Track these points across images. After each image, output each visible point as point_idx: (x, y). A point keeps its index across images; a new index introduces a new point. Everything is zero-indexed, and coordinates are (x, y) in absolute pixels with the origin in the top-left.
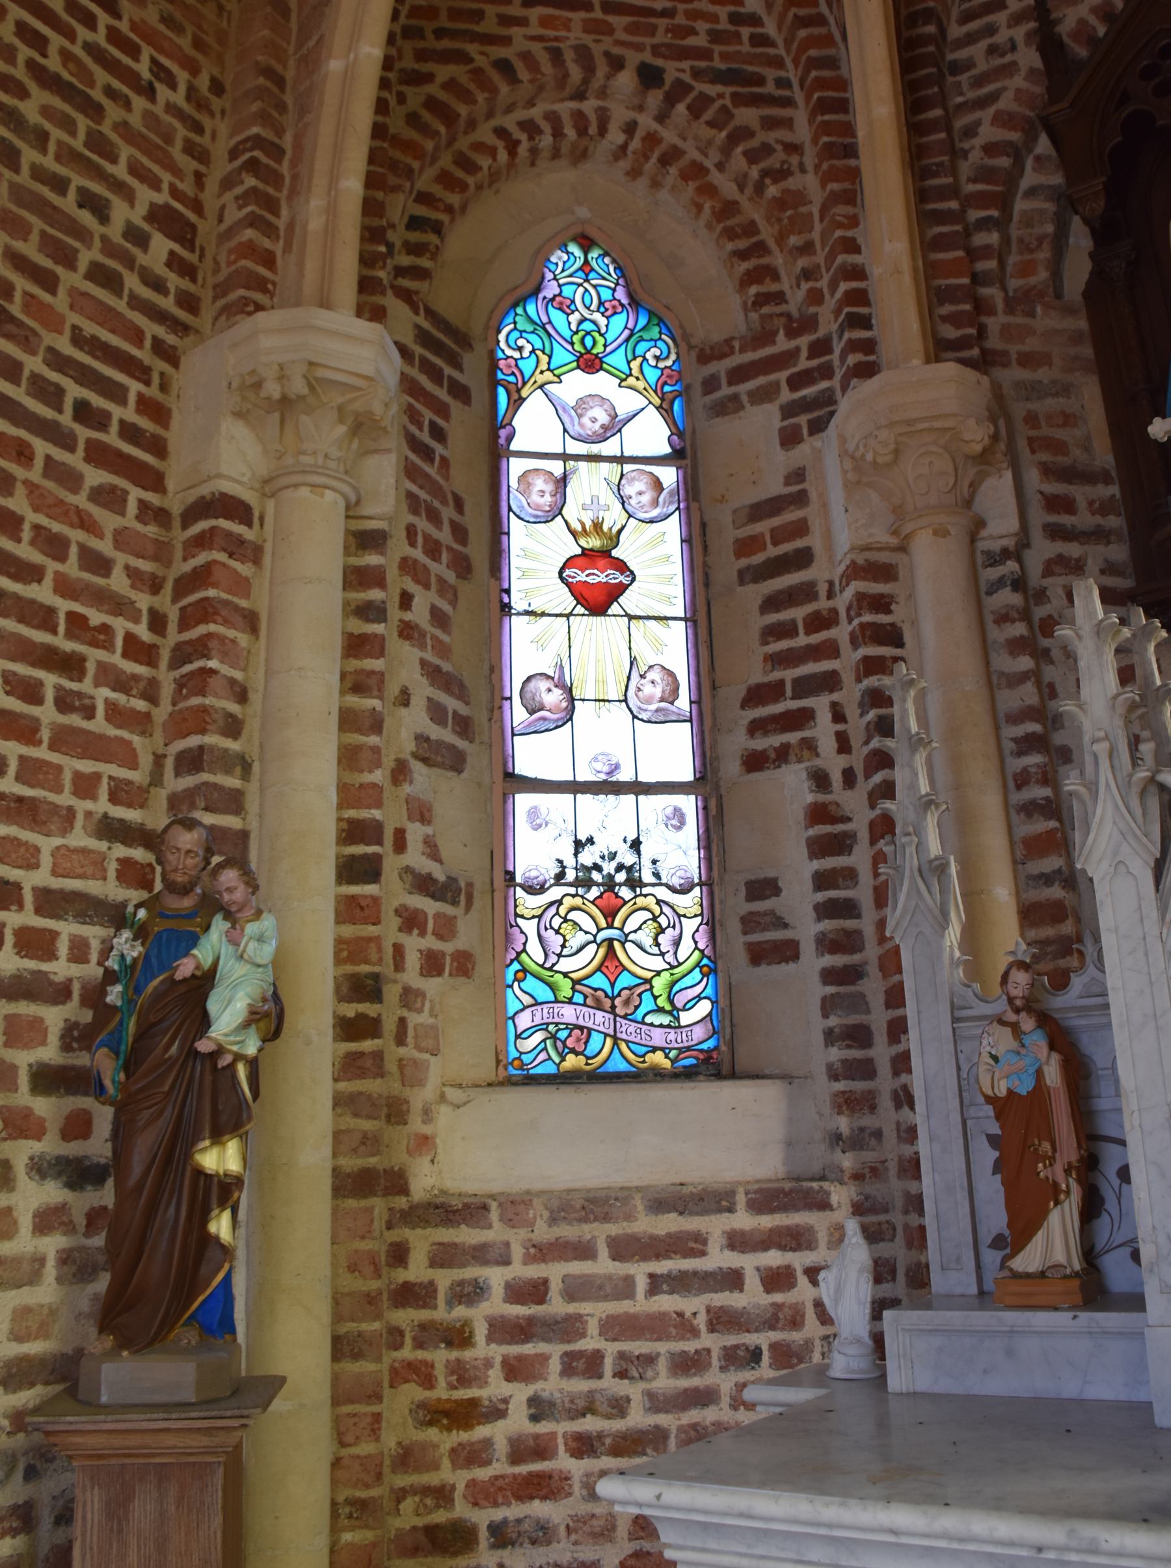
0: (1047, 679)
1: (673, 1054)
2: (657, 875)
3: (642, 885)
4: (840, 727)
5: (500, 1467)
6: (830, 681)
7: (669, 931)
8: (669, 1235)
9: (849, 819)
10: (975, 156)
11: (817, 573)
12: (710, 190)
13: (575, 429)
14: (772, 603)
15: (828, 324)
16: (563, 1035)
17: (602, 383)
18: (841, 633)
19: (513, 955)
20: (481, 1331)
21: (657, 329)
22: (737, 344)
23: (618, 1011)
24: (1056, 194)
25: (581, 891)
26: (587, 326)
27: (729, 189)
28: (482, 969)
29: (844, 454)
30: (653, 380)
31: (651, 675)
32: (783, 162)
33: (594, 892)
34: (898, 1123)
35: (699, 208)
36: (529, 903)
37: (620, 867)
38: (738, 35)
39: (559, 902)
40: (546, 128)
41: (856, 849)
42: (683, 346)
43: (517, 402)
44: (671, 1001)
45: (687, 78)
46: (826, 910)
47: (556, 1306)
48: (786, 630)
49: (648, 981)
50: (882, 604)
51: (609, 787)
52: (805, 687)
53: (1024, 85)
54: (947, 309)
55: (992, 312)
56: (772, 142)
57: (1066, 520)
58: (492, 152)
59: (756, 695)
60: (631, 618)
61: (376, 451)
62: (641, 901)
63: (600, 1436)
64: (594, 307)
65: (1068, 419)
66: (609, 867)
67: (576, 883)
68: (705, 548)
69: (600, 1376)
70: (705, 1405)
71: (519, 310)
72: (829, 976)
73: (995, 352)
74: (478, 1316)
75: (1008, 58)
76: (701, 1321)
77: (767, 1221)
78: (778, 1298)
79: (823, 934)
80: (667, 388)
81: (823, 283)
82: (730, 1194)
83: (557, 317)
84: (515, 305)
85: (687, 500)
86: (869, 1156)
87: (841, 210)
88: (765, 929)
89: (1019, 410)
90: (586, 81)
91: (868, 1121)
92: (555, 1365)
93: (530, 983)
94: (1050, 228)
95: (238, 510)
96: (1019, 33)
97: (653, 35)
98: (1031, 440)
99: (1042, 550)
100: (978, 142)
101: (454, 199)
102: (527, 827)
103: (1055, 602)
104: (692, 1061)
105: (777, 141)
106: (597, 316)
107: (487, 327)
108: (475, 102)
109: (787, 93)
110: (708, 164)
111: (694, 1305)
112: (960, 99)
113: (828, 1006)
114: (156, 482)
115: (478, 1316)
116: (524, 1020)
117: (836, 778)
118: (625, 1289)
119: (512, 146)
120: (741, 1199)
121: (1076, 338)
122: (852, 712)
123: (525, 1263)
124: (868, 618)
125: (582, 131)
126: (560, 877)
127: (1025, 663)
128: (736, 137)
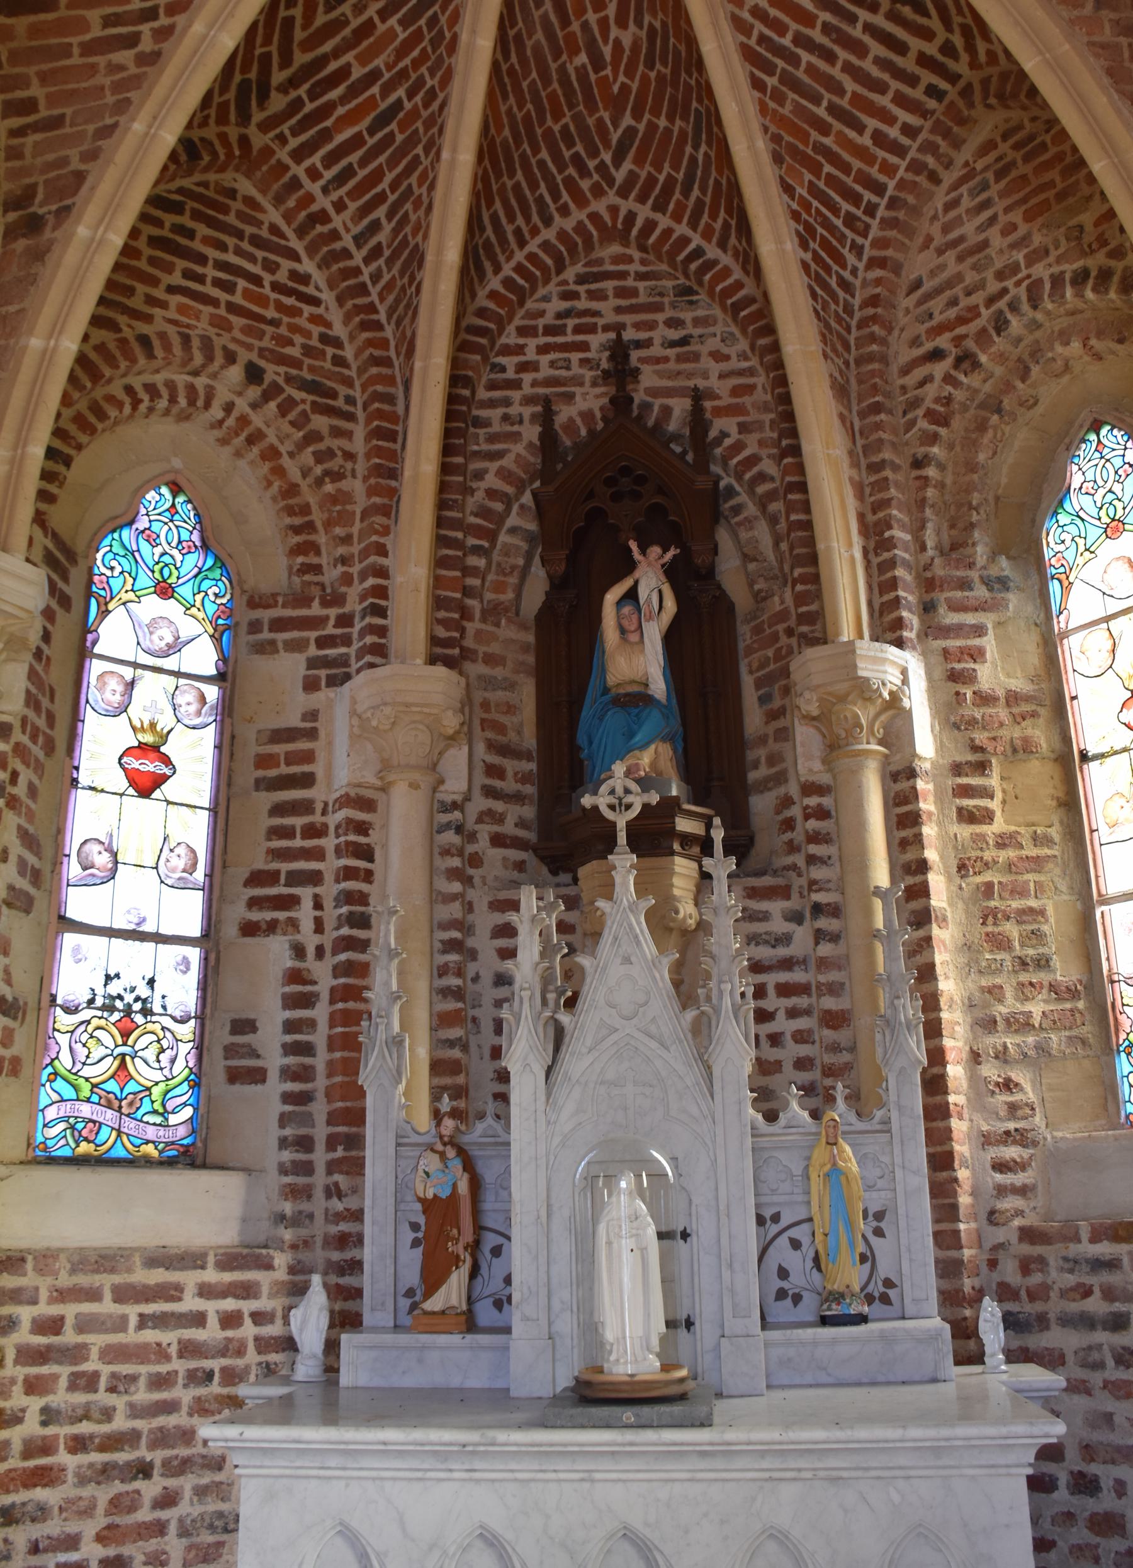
0: (468, 898)
1: (161, 1146)
2: (164, 1007)
3: (152, 1014)
4: (318, 913)
6: (315, 878)
7: (168, 1052)
8: (157, 1285)
9: (315, 983)
10: (480, 495)
12: (279, 471)
13: (146, 644)
14: (278, 810)
15: (353, 605)
16: (80, 1126)
17: (171, 609)
18: (329, 843)
19: (48, 1061)
21: (219, 571)
22: (280, 600)
23: (124, 1110)
24: (530, 538)
25: (106, 1014)
26: (167, 559)
27: (294, 474)
28: (26, 1071)
29: (353, 713)
30: (210, 612)
31: (177, 851)
32: (341, 467)
33: (116, 1016)
34: (327, 1210)
35: (269, 484)
36: (64, 1020)
37: (137, 999)
38: (323, 353)
39: (88, 1022)
40: (165, 393)
41: (318, 1005)
42: (237, 589)
43: (104, 613)
44: (164, 1105)
45: (281, 381)
46: (291, 1049)
47: (69, 1337)
49: (148, 1089)
50: (362, 828)
51: (136, 935)
52: (296, 878)
53: (524, 453)
54: (442, 614)
55: (471, 619)
56: (335, 448)
57: (497, 783)
58: (120, 405)
59: (257, 878)
60: (169, 803)
61: (14, 660)
62: (150, 1027)
63: (92, 1437)
64: (174, 544)
65: (510, 709)
66: (129, 998)
67: (103, 1008)
68: (232, 755)
69: (96, 1391)
70: (170, 1413)
71: (116, 535)
73: (469, 650)
75: (516, 428)
76: (173, 1350)
77: (228, 1277)
78: (230, 1333)
79: (288, 1066)
80: (220, 622)
81: (355, 570)
82: (203, 1256)
83: (145, 547)
84: (114, 531)
85: (223, 714)
86: (304, 1232)
87: (379, 519)
88: (242, 1057)
89: (478, 696)
90: (204, 366)
91: (305, 1206)
92: (63, 1383)
93: (59, 1084)
94: (521, 562)
96: (527, 411)
97: (261, 339)
98: (483, 721)
99: (478, 803)
100: (483, 485)
101: (83, 438)
102: (71, 960)
103: (481, 843)
104: (174, 1153)
105: (340, 448)
106: (175, 552)
107: (89, 546)
108: (117, 367)
109: (351, 409)
110: (283, 449)
111: (169, 1338)
112: (476, 448)
116: (51, 1113)
117: (311, 951)
118: (121, 1324)
119: (136, 403)
120: (211, 1260)
121: (525, 648)
122: (329, 903)
123: (49, 1303)
124: (352, 838)
125: (192, 402)
126: (91, 1001)
127: (456, 887)
128: (313, 437)
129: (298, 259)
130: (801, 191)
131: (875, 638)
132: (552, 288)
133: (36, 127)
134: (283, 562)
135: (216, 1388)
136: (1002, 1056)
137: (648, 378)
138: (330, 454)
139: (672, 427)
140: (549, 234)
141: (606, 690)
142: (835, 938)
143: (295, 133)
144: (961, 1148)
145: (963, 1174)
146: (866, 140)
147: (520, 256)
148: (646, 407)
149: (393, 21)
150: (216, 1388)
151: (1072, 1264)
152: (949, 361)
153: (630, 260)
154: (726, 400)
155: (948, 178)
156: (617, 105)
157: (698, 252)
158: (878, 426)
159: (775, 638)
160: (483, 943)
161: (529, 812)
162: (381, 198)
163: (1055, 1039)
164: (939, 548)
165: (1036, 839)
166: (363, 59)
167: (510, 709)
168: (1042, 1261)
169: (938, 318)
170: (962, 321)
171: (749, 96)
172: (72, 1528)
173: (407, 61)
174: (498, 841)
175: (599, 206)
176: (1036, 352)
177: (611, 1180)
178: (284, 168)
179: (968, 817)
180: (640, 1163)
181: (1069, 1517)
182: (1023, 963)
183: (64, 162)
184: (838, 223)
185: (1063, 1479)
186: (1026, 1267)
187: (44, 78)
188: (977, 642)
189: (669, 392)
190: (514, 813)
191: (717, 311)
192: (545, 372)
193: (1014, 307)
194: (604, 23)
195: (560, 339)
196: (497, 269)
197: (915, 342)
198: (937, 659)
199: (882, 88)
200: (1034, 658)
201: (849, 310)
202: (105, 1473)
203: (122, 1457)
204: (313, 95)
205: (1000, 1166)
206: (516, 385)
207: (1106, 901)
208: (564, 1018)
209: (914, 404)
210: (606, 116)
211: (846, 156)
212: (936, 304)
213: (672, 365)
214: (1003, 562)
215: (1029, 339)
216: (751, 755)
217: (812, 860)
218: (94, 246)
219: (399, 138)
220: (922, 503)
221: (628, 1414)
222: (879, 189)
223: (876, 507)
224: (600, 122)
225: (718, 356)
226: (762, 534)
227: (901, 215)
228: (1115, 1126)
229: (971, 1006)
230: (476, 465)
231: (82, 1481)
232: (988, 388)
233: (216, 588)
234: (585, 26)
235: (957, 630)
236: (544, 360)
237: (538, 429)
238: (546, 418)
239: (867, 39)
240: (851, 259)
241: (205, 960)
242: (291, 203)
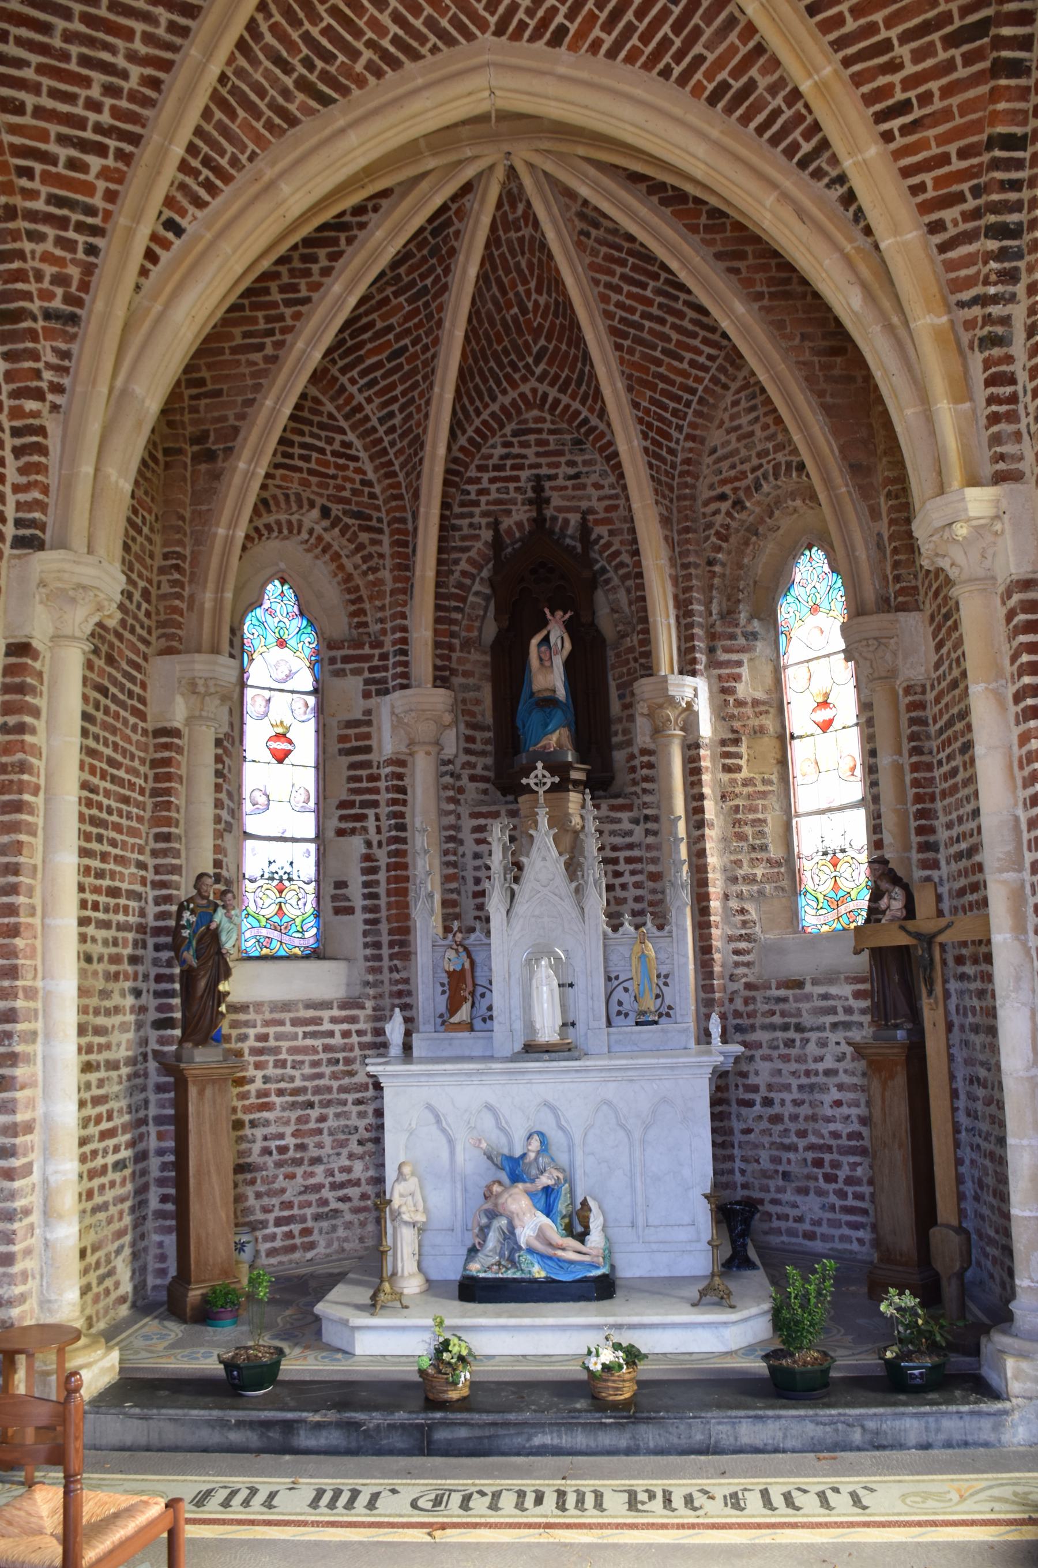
5: (253, 1100)
6: (375, 804)
10: (457, 574)
11: (372, 757)
12: (341, 567)
14: (353, 766)
18: (382, 784)
20: (246, 1052)
24: (487, 598)
29: (393, 713)
46: (366, 896)
47: (272, 1043)
48: (358, 779)
50: (400, 777)
52: (364, 804)
59: (343, 805)
74: (246, 1046)
77: (344, 1013)
81: (388, 625)
83: (269, 618)
87: (401, 597)
91: (379, 977)
95: (176, 733)
96: (484, 521)
99: (464, 758)
100: (459, 568)
111: (318, 1043)
113: (365, 934)
115: (246, 1046)
117: (375, 844)
118: (295, 1037)
121: (485, 665)
122: (383, 818)
125: (291, 531)
127: (452, 807)
128: (361, 547)
129: (344, 433)
131: (681, 673)
132: (497, 439)
134: (345, 620)
135: (341, 1067)
136: (740, 896)
137: (556, 500)
138: (370, 556)
139: (570, 531)
141: (532, 694)
142: (655, 833)
143: (341, 358)
144: (717, 943)
145: (717, 956)
146: (685, 365)
148: (554, 519)
149: (402, 299)
150: (341, 1067)
151: (767, 1000)
152: (729, 503)
153: (543, 420)
154: (602, 515)
155: (734, 386)
156: (537, 333)
158: (687, 541)
159: (627, 662)
160: (468, 838)
161: (489, 761)
162: (395, 399)
163: (768, 888)
165: (764, 782)
168: (754, 998)
169: (725, 475)
170: (737, 479)
171: (612, 356)
172: (281, 1130)
173: (410, 324)
174: (473, 778)
175: (525, 388)
176: (778, 502)
178: (335, 379)
179: (728, 769)
180: (550, 953)
181: (760, 1117)
182: (753, 848)
183: (225, 418)
184: (668, 415)
185: (758, 1100)
186: (746, 1001)
188: (737, 670)
189: (569, 509)
190: (481, 762)
191: (597, 456)
192: (494, 495)
193: (765, 477)
194: (528, 293)
195: (502, 474)
196: (464, 432)
197: (712, 487)
198: (715, 680)
199: (694, 335)
200: (769, 680)
201: (673, 466)
202: (293, 1106)
203: (300, 1099)
206: (476, 503)
207: (798, 816)
208: (515, 886)
209: (709, 526)
210: (530, 339)
211: (672, 376)
212: (725, 465)
213: (570, 492)
214: (756, 623)
216: (614, 728)
217: (645, 791)
218: (248, 476)
219: (406, 368)
220: (711, 587)
222: (693, 391)
224: (526, 342)
225: (597, 486)
227: (705, 410)
228: (796, 932)
229: (725, 870)
230: (455, 555)
231: (284, 1109)
233: (309, 640)
234: (517, 294)
235: (727, 664)
236: (493, 487)
237: (491, 533)
238: (495, 526)
239: (685, 309)
240: (675, 434)
241: (318, 850)
242: (341, 401)
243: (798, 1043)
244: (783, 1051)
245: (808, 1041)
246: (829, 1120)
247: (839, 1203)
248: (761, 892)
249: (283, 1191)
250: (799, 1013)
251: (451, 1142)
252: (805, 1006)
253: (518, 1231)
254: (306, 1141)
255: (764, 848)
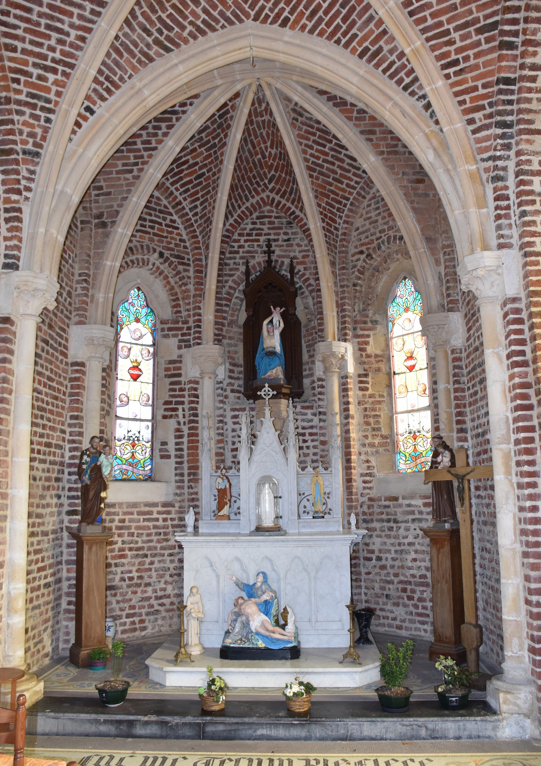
5: (116, 553)
6: (183, 403)
10: (227, 288)
12: (168, 283)
14: (172, 383)
15: (191, 324)
17: (139, 326)
18: (186, 393)
20: (114, 528)
36: (118, 443)
43: (122, 329)
46: (177, 450)
47: (127, 523)
48: (174, 390)
50: (196, 389)
52: (177, 403)
57: (232, 375)
72: (177, 463)
77: (164, 509)
83: (131, 307)
96: (241, 261)
99: (228, 381)
100: (228, 285)
111: (150, 524)
113: (176, 469)
114: (65, 355)
117: (182, 423)
118: (139, 521)
121: (240, 334)
122: (186, 410)
125: (143, 264)
127: (221, 405)
128: (178, 273)
130: (323, 205)
132: (249, 220)
133: (102, 194)
134: (169, 310)
135: (162, 537)
138: (183, 277)
140: (248, 204)
141: (263, 349)
142: (324, 421)
143: (171, 177)
146: (344, 186)
147: (239, 212)
148: (276, 261)
149: (203, 149)
150: (162, 537)
151: (380, 506)
152: (365, 255)
153: (273, 212)
154: (301, 260)
155: (368, 197)
156: (270, 168)
157: (293, 213)
159: (312, 334)
161: (241, 382)
162: (198, 199)
164: (359, 311)
166: (193, 158)
167: (236, 352)
169: (363, 241)
170: (369, 243)
172: (130, 568)
173: (207, 162)
174: (232, 391)
175: (264, 195)
177: (264, 484)
179: (361, 389)
183: (112, 206)
184: (335, 211)
185: (374, 558)
186: (369, 508)
187: (105, 180)
189: (283, 257)
190: (237, 383)
191: (299, 230)
192: (247, 249)
193: (383, 242)
194: (266, 148)
196: (232, 216)
197: (356, 247)
199: (349, 171)
200: (383, 345)
203: (141, 553)
204: (177, 167)
205: (365, 482)
206: (237, 252)
207: (397, 413)
209: (354, 267)
210: (266, 171)
211: (337, 191)
212: (363, 236)
213: (284, 248)
214: (377, 316)
215: (387, 251)
216: (304, 367)
219: (204, 183)
221: (267, 533)
222: (348, 199)
223: (342, 299)
224: (265, 172)
225: (299, 245)
226: (310, 301)
227: (354, 208)
232: (376, 263)
234: (261, 148)
236: (246, 244)
237: (245, 267)
239: (345, 158)
241: (153, 425)
243: (395, 529)
244: (387, 532)
245: (400, 528)
246: (410, 568)
247: (415, 611)
248: (377, 452)
249: (131, 600)
250: (395, 514)
251: (218, 576)
252: (399, 510)
253: (251, 623)
254: (143, 574)
255: (379, 429)
